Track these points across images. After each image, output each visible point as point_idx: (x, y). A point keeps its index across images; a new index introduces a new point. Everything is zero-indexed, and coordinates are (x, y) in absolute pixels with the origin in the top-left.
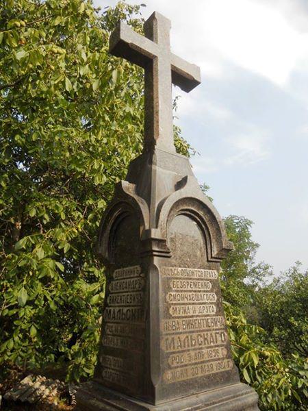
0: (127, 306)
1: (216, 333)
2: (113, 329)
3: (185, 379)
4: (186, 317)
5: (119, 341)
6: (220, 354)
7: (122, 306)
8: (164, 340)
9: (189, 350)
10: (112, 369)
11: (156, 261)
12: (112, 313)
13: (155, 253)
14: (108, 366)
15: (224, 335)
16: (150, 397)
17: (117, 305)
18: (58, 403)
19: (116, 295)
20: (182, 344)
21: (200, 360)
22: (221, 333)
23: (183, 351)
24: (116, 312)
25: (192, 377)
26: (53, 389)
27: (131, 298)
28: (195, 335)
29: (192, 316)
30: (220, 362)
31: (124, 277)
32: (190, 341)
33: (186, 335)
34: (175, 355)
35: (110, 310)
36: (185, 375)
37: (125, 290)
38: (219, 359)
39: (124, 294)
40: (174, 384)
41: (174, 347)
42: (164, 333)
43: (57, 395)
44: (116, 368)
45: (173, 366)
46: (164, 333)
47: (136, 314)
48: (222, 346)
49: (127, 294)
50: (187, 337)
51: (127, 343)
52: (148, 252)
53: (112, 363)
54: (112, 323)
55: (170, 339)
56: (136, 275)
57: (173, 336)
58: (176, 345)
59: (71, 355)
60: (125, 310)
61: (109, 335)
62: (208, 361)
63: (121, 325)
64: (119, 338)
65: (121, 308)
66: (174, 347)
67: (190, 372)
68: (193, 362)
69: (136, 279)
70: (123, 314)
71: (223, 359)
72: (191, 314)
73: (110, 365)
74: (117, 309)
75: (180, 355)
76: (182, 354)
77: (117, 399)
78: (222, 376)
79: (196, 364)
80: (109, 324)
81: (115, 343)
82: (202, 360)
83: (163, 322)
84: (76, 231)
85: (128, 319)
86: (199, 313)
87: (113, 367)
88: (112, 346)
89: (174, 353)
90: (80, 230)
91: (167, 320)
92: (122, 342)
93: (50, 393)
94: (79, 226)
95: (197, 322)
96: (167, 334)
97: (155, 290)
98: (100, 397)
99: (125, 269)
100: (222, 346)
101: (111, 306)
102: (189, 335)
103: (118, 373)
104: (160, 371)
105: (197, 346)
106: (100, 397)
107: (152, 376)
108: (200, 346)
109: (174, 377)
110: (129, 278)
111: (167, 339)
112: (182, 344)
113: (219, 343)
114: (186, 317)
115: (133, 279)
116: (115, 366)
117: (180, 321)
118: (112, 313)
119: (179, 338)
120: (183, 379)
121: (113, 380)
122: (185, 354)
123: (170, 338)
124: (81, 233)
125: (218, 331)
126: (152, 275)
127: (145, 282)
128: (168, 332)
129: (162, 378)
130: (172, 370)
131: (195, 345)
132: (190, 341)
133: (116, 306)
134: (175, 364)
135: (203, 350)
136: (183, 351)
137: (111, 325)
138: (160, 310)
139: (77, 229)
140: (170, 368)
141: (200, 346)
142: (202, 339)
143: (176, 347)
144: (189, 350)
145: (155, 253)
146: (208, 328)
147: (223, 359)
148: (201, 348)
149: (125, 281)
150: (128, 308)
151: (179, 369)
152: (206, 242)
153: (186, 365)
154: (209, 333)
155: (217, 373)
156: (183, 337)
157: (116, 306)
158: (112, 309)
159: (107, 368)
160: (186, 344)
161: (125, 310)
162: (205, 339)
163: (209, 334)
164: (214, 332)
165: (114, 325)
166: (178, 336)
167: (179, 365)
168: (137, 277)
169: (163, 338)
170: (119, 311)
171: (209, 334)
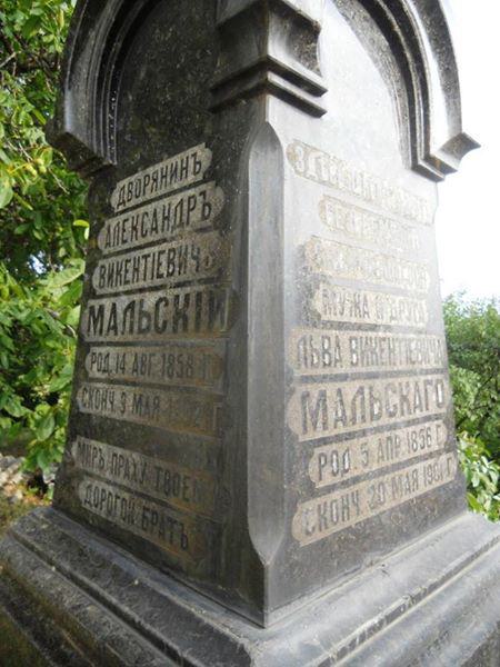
0: (156, 289)
1: (427, 382)
2: (112, 362)
3: (353, 521)
4: (360, 327)
5: (130, 401)
6: (434, 442)
7: (141, 290)
8: (297, 397)
9: (364, 433)
10: (108, 482)
11: (277, 113)
12: (107, 314)
13: (274, 79)
14: (96, 471)
15: (442, 386)
16: (246, 587)
17: (121, 289)
18: (24, 495)
19: (120, 259)
20: (348, 413)
21: (391, 462)
22: (438, 381)
23: (350, 436)
24: (120, 311)
25: (371, 514)
26: (15, 472)
27: (170, 262)
28: (379, 384)
29: (374, 328)
30: (431, 462)
31: (149, 196)
32: (367, 403)
33: (357, 384)
34: (326, 449)
35: (102, 308)
36: (109, 406)
37: (150, 238)
38: (431, 455)
39: (146, 251)
40: (323, 543)
41: (325, 424)
42: (297, 374)
43: (22, 482)
44: (121, 480)
45: (320, 485)
46: (297, 374)
47: (191, 313)
48: (437, 417)
49: (156, 249)
50: (361, 391)
51: (157, 406)
52: (247, 74)
53: (107, 464)
54: (110, 344)
55: (315, 394)
56: (191, 178)
57: (322, 387)
58: (332, 416)
59: (36, 421)
60: (150, 300)
61: (99, 380)
62: (410, 462)
63: (138, 349)
64: (126, 389)
65: (136, 297)
66: (325, 424)
67: (365, 499)
68: (375, 467)
69: (191, 192)
70: (142, 314)
71: (439, 453)
72: (371, 320)
73: (102, 468)
74: (123, 302)
75: (340, 447)
76: (346, 444)
77: (124, 580)
78: (436, 501)
79: (382, 472)
80: (97, 350)
81: (115, 404)
82: (396, 460)
83: (294, 336)
84: (35, 172)
85: (160, 331)
86: (392, 318)
87: (108, 475)
88: (106, 413)
89: (324, 441)
90: (43, 169)
91: (308, 332)
92: (138, 403)
93: (9, 478)
94: (41, 161)
95: (385, 346)
96: (306, 379)
97: (267, 217)
98: (67, 567)
99: (150, 170)
100: (437, 417)
101: (102, 296)
102: (366, 383)
103: (126, 495)
104: (282, 507)
105: (385, 420)
106: (67, 567)
107: (250, 521)
108: (393, 420)
109: (323, 523)
110: (166, 195)
111: (306, 396)
112: (348, 413)
113: (433, 410)
114: (360, 327)
115: (179, 197)
116: (115, 471)
117: (344, 336)
118: (107, 314)
119: (339, 391)
120: (347, 524)
121: (109, 512)
122: (356, 443)
123: (314, 390)
124: (48, 177)
125: (429, 377)
126: (256, 165)
127: (230, 194)
128: (310, 372)
129: (289, 529)
130: (319, 501)
131: (379, 417)
132: (367, 403)
133: (116, 295)
134: (328, 480)
135: (398, 432)
136: (350, 436)
137: (103, 350)
138: (287, 294)
139: (37, 167)
140: (312, 492)
141: (393, 420)
142: (396, 400)
143: (331, 423)
144: (364, 433)
145: (274, 79)
146: (410, 367)
147: (439, 453)
148: (394, 427)
149: (149, 208)
150: (160, 294)
151: (336, 495)
152: (412, 111)
153: (356, 480)
154: (412, 380)
155: (426, 495)
156: (350, 389)
157: (116, 295)
158: (107, 303)
159: (90, 475)
160: (359, 415)
161: (150, 300)
162: (404, 399)
163: (412, 386)
164: (423, 378)
165: (112, 350)
166: (339, 385)
167: (338, 479)
168: (195, 184)
169: (292, 391)
170: (131, 306)
171: (412, 386)
